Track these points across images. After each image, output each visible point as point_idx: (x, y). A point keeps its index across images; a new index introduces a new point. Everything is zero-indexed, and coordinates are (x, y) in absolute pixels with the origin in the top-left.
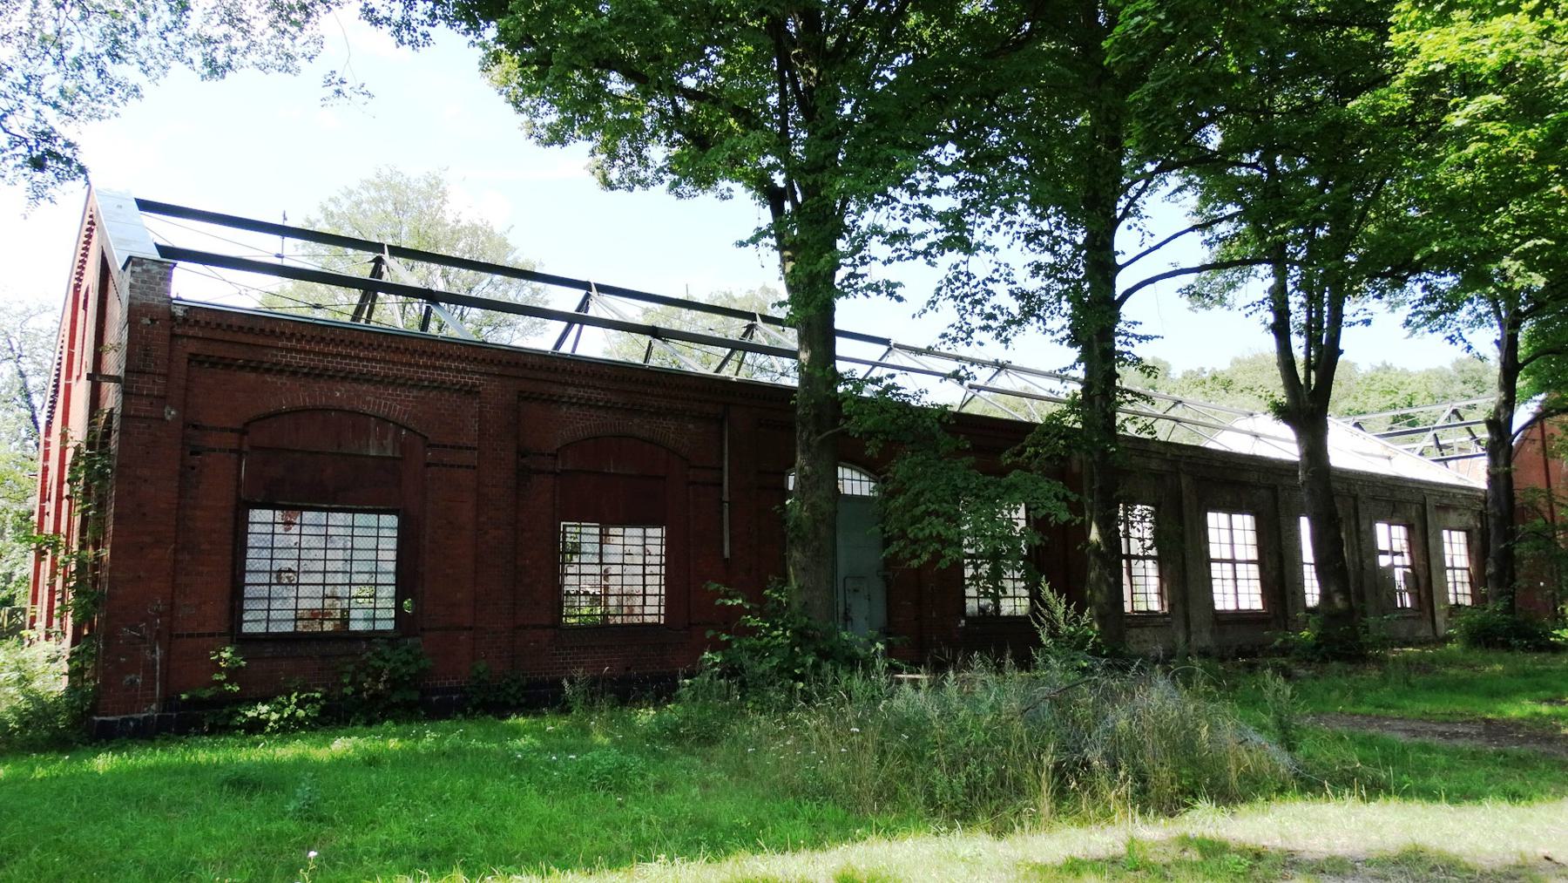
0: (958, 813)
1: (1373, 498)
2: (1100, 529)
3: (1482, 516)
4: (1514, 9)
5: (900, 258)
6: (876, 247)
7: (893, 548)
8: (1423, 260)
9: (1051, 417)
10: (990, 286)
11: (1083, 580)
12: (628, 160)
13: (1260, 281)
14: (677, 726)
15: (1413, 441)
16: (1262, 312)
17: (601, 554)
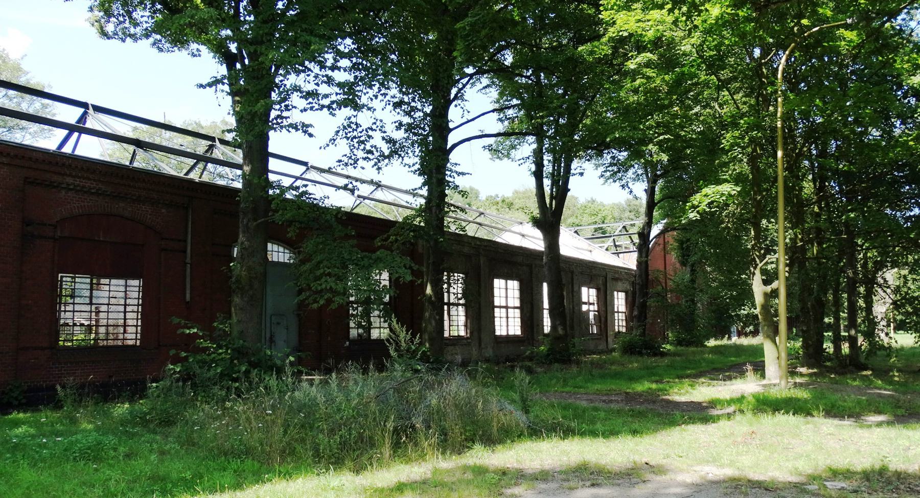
0: (333, 460)
1: (581, 273)
2: (432, 287)
3: (633, 284)
4: (661, 7)
5: (312, 108)
6: (296, 100)
7: (303, 296)
8: (611, 141)
9: (406, 218)
10: (370, 133)
11: (421, 317)
12: (121, 19)
13: (528, 147)
14: (146, 414)
15: (603, 242)
16: (527, 164)
17: (91, 297)
